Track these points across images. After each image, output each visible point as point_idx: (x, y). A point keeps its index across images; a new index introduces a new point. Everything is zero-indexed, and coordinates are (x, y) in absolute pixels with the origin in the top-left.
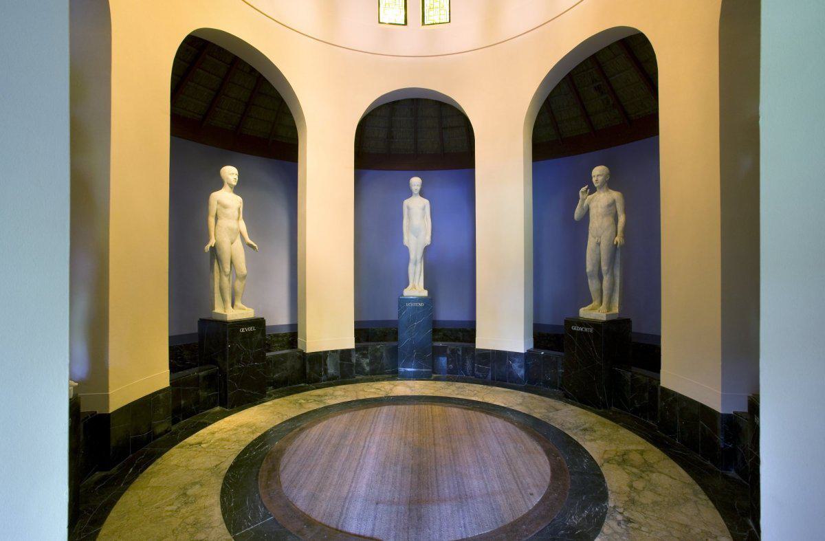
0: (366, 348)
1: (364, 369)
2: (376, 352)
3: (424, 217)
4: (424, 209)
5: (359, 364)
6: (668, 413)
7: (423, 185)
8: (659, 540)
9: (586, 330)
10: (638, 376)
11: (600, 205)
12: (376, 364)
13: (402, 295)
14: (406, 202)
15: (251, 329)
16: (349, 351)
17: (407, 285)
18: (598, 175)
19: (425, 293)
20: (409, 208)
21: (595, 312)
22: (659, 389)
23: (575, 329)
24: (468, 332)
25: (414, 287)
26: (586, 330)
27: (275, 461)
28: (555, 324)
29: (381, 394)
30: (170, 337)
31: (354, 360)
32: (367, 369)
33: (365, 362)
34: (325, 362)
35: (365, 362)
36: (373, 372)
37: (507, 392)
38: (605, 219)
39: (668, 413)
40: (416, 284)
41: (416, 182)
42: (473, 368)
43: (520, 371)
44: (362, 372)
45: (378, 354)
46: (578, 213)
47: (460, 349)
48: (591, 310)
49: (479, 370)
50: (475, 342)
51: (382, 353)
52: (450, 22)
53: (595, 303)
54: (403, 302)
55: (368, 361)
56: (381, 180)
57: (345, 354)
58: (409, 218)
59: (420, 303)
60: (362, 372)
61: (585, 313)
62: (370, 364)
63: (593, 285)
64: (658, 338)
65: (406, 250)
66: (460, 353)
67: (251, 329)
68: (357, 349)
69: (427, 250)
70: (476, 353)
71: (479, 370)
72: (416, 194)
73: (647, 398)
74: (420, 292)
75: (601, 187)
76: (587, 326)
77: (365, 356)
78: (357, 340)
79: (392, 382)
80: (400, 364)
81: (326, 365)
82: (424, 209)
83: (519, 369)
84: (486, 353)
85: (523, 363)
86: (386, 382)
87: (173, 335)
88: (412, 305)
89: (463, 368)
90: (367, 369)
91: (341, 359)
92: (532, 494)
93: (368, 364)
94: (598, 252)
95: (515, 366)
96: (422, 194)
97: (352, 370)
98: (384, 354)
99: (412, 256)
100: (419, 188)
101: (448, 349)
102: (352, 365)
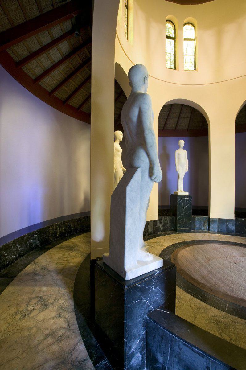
14: (177, 152)
15: (188, 199)
16: (156, 221)
19: (187, 194)
20: (179, 154)
27: (173, 266)
29: (191, 239)
31: (158, 225)
32: (162, 229)
34: (148, 226)
38: (142, 91)
41: (182, 143)
43: (232, 227)
44: (160, 231)
45: (166, 222)
51: (168, 221)
52: (175, 69)
55: (162, 225)
57: (155, 222)
58: (178, 159)
59: (187, 198)
60: (160, 231)
62: (163, 226)
67: (188, 199)
68: (160, 219)
78: (159, 216)
80: (178, 225)
81: (148, 228)
85: (234, 224)
88: (184, 199)
90: (162, 229)
91: (154, 225)
95: (230, 225)
96: (184, 148)
100: (183, 145)
101: (196, 219)
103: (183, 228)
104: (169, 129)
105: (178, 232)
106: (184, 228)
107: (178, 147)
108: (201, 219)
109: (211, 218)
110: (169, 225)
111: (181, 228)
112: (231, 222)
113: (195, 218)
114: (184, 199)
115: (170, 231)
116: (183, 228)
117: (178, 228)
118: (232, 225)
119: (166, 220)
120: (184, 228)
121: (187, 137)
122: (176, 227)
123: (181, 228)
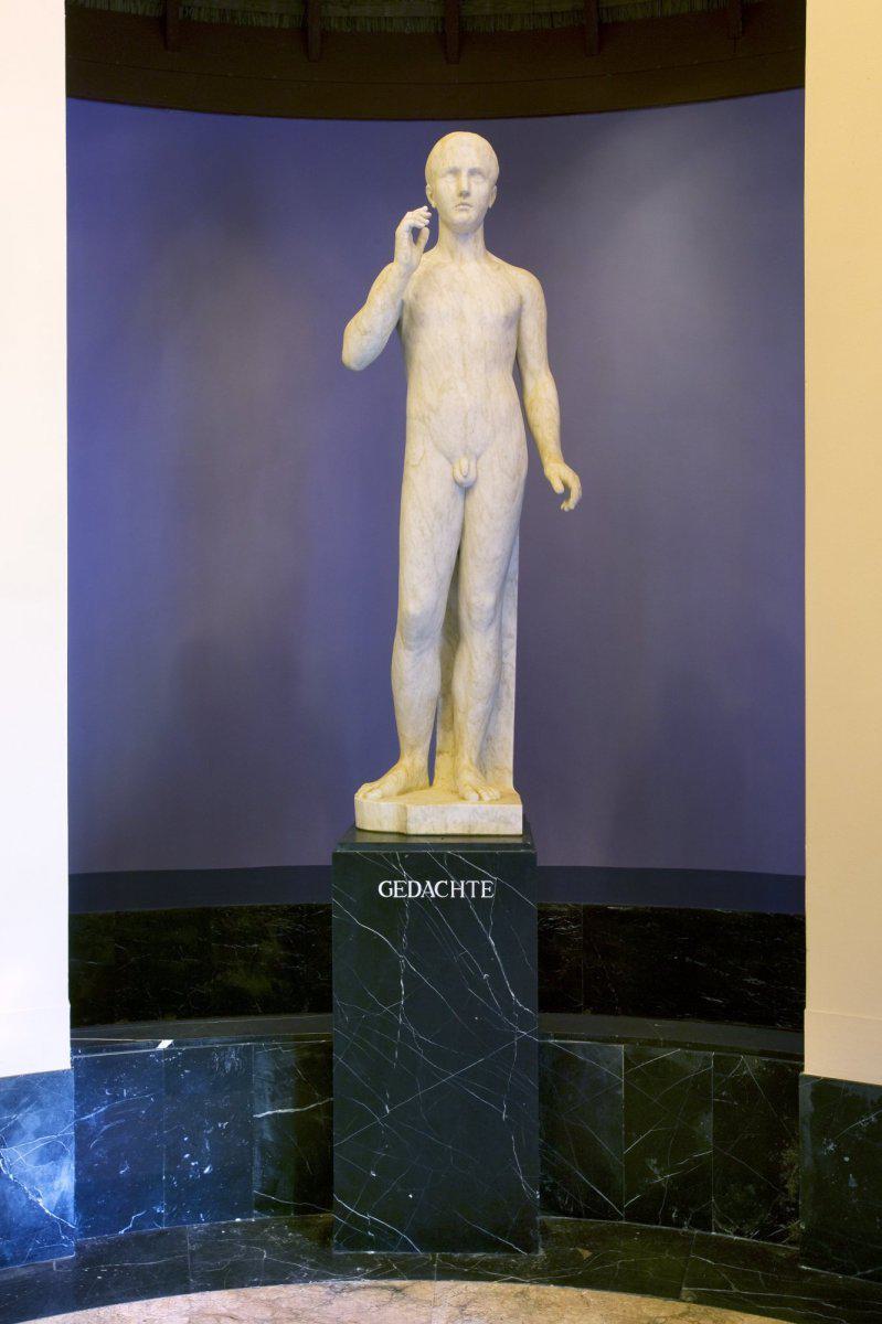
6: (853, 1183)
7: (511, 187)
9: (458, 888)
10: (668, 1054)
11: (458, 319)
18: (472, 172)
21: (450, 789)
22: (805, 1093)
23: (395, 892)
26: (458, 888)
28: (96, 870)
37: (365, 1288)
39: (853, 1183)
41: (462, 162)
46: (362, 338)
48: (404, 791)
53: (412, 760)
61: (381, 808)
63: (413, 674)
64: (795, 886)
73: (709, 1138)
75: (462, 232)
76: (462, 873)
82: (515, 321)
83: (47, 1167)
94: (456, 526)
112: (30, 1120)
118: (51, 1155)
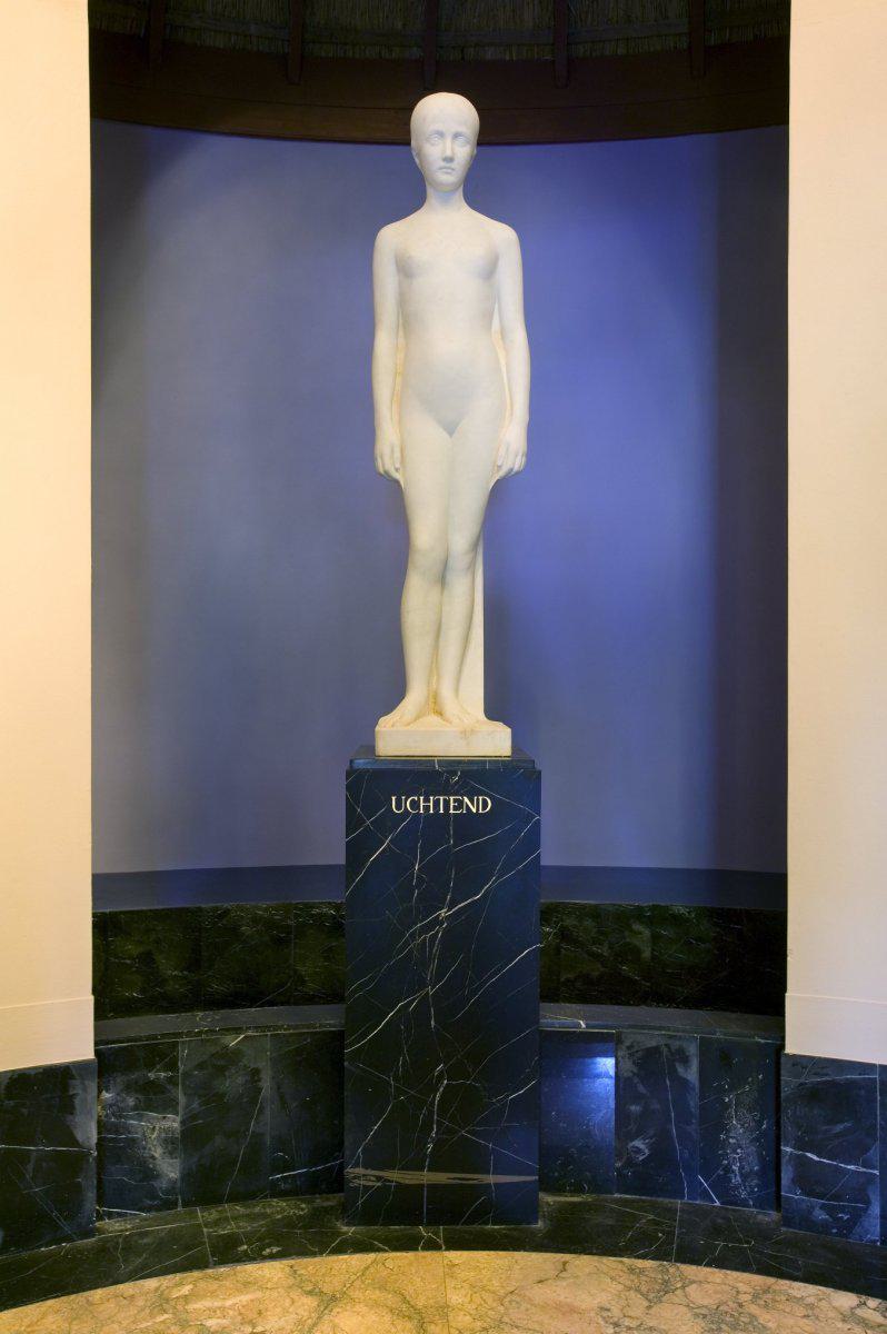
0: (158, 1052)
1: (148, 1173)
2: (221, 1070)
3: (487, 316)
4: (489, 272)
5: (116, 1146)
8: (709, 1332)
12: (219, 1141)
13: (372, 748)
14: (392, 237)
16: (52, 1083)
17: (395, 692)
19: (496, 742)
20: (405, 269)
24: (733, 941)
25: (435, 705)
30: (93, 876)
31: (88, 1134)
32: (170, 1170)
33: (156, 1131)
35: (156, 1131)
36: (203, 1188)
40: (446, 692)
42: (773, 1165)
44: (135, 1189)
45: (232, 1084)
47: (692, 1050)
49: (809, 1180)
50: (778, 1009)
51: (256, 1072)
54: (376, 784)
55: (173, 1122)
56: (229, 195)
58: (408, 322)
60: (135, 1189)
65: (391, 500)
66: (692, 1074)
68: (108, 1061)
69: (501, 495)
70: (788, 1081)
71: (809, 1180)
72: (445, 196)
74: (466, 734)
77: (154, 1097)
78: (108, 1002)
79: (311, 1266)
82: (489, 272)
84: (852, 1084)
86: (272, 1272)
87: (97, 872)
88: (426, 804)
89: (710, 1158)
90: (170, 1170)
92: (527, 1310)
93: (170, 1144)
96: (480, 192)
97: (78, 1189)
98: (266, 1084)
99: (424, 533)
100: (463, 151)
102: (75, 1162)
103: (427, 1177)
104: (490, 54)
105: (367, 1216)
106: (442, 1178)
107: (410, 194)
108: (685, 1061)
109: (801, 1062)
110: (268, 1121)
111: (395, 1176)
113: (177, 1114)
114: (426, 804)
115: (282, 1194)
116: (427, 1177)
117: (360, 1175)
119: (230, 1058)
120: (442, 1178)
121: (683, 143)
122: (333, 1147)
123: (395, 1176)
